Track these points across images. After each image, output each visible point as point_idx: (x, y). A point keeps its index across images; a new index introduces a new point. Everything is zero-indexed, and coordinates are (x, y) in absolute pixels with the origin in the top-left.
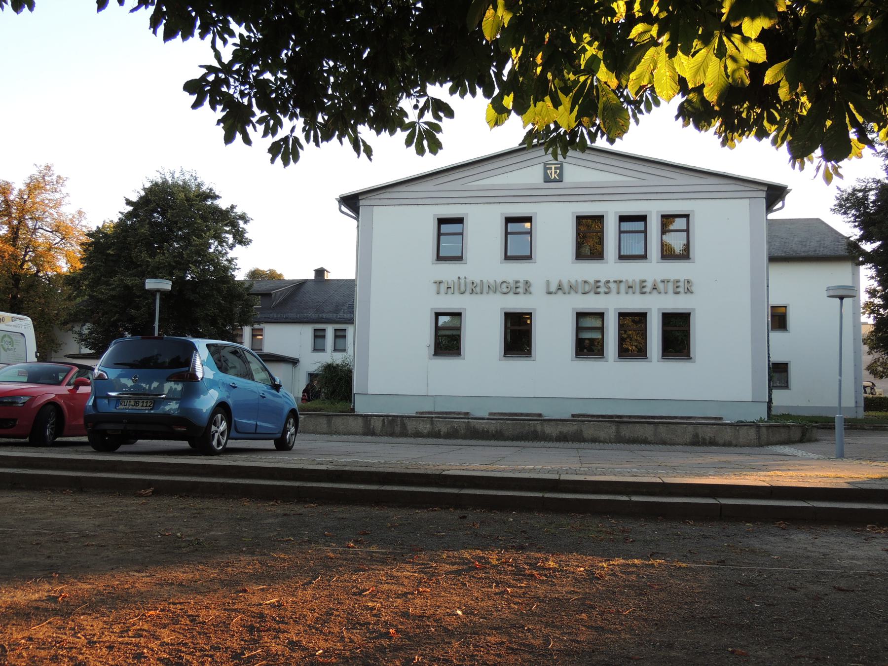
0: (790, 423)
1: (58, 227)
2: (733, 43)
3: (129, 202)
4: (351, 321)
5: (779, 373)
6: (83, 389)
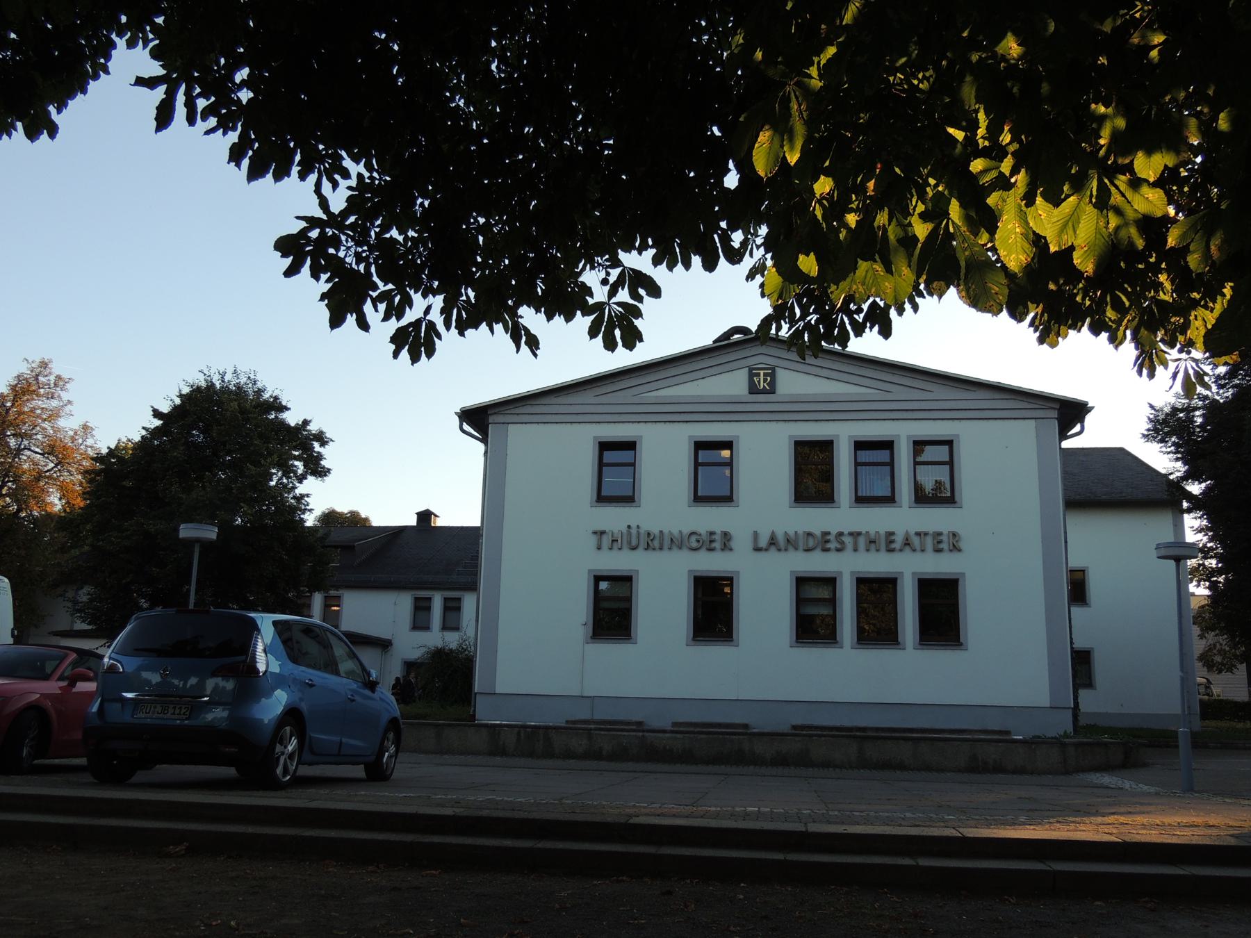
0: (1105, 738)
1: (52, 447)
2: (1117, 187)
3: (157, 414)
4: (473, 587)
5: (1082, 661)
6: (82, 686)
